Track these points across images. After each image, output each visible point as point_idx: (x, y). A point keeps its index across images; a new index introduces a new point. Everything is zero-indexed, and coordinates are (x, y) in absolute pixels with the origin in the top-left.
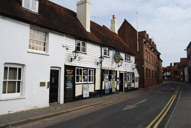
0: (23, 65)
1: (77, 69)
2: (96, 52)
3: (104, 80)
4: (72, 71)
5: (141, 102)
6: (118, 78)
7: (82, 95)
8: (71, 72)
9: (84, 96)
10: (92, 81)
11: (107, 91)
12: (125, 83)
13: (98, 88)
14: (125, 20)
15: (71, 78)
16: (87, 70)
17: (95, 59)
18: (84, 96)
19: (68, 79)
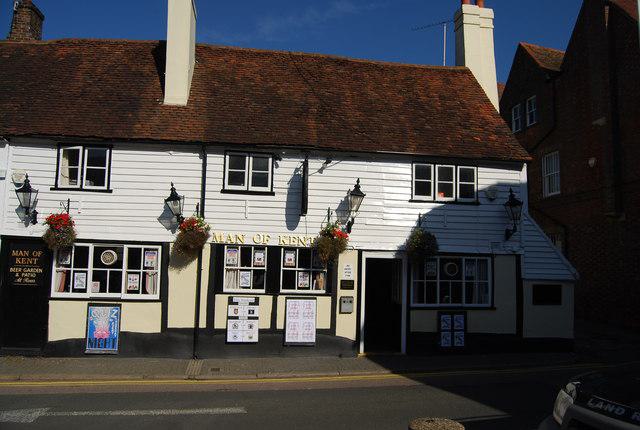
0: (224, 191)
1: (88, 247)
2: (135, 192)
3: (225, 290)
4: (39, 254)
5: (174, 412)
6: (347, 285)
7: (436, 336)
8: (31, 256)
9: (445, 342)
10: (154, 292)
11: (104, 342)
12: (409, 309)
13: (182, 316)
14: (521, 49)
15: (31, 278)
16: (120, 253)
17: (386, 196)
18: (445, 342)
19: (19, 280)
